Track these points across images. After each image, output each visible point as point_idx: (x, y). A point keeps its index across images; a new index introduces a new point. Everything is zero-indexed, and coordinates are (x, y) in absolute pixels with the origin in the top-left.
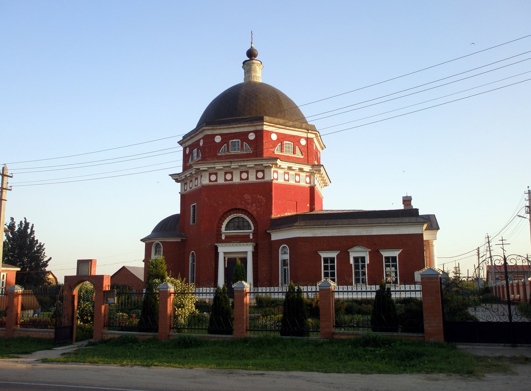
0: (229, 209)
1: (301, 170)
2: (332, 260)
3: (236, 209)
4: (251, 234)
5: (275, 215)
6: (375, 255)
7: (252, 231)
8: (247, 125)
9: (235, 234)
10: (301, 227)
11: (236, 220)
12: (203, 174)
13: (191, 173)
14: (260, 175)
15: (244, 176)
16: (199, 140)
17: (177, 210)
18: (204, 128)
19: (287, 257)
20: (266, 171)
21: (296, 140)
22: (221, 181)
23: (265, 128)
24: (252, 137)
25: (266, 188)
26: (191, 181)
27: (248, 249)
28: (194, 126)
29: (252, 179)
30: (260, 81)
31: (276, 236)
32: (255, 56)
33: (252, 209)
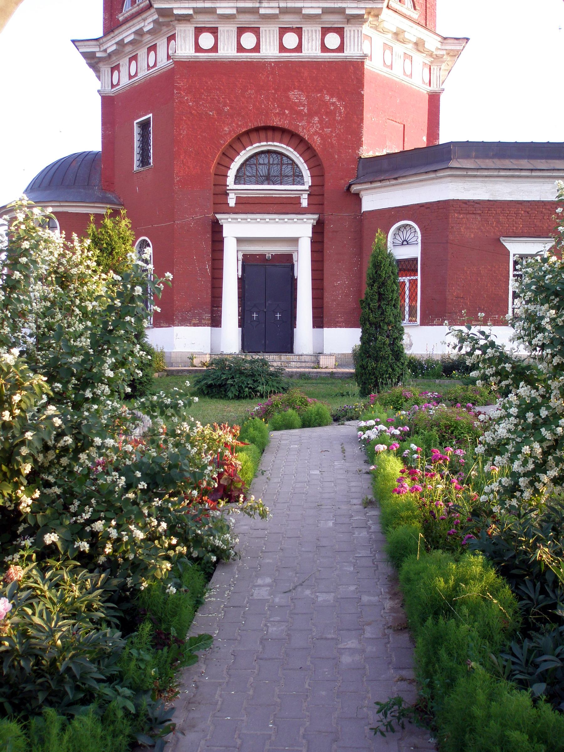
0: (251, 126)
1: (419, 45)
3: (266, 128)
4: (306, 196)
5: (367, 152)
7: (306, 187)
9: (261, 194)
10: (466, 174)
11: (263, 159)
13: (137, 33)
14: (333, 40)
15: (290, 40)
20: (349, 31)
22: (227, 50)
26: (134, 58)
27: (300, 230)
29: (311, 50)
31: (374, 200)
33: (309, 130)
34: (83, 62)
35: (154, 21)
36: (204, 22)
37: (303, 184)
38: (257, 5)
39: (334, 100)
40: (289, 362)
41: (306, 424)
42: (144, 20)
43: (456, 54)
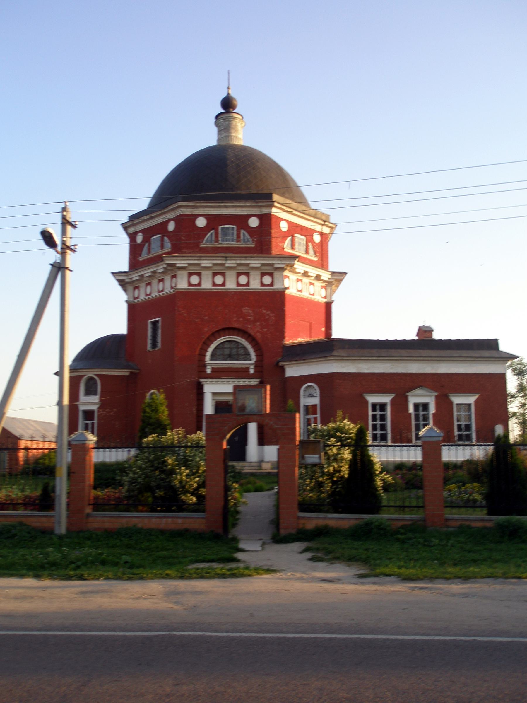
1: (318, 278)
2: (383, 407)
5: (289, 341)
6: (444, 402)
8: (248, 204)
10: (341, 359)
11: (227, 345)
12: (179, 273)
14: (267, 280)
15: (243, 280)
16: (167, 222)
17: (121, 328)
18: (181, 203)
19: (315, 401)
20: (276, 274)
21: (308, 233)
22: (207, 285)
23: (275, 211)
24: (254, 222)
25: (277, 300)
28: (144, 205)
29: (255, 285)
30: (242, 143)
31: (293, 371)
32: (234, 107)
33: (255, 330)
34: (116, 283)
35: (165, 268)
36: (193, 270)
37: (250, 360)
38: (224, 262)
39: (268, 313)
40: (243, 467)
41: (257, 490)
42: (158, 266)
43: (340, 281)
